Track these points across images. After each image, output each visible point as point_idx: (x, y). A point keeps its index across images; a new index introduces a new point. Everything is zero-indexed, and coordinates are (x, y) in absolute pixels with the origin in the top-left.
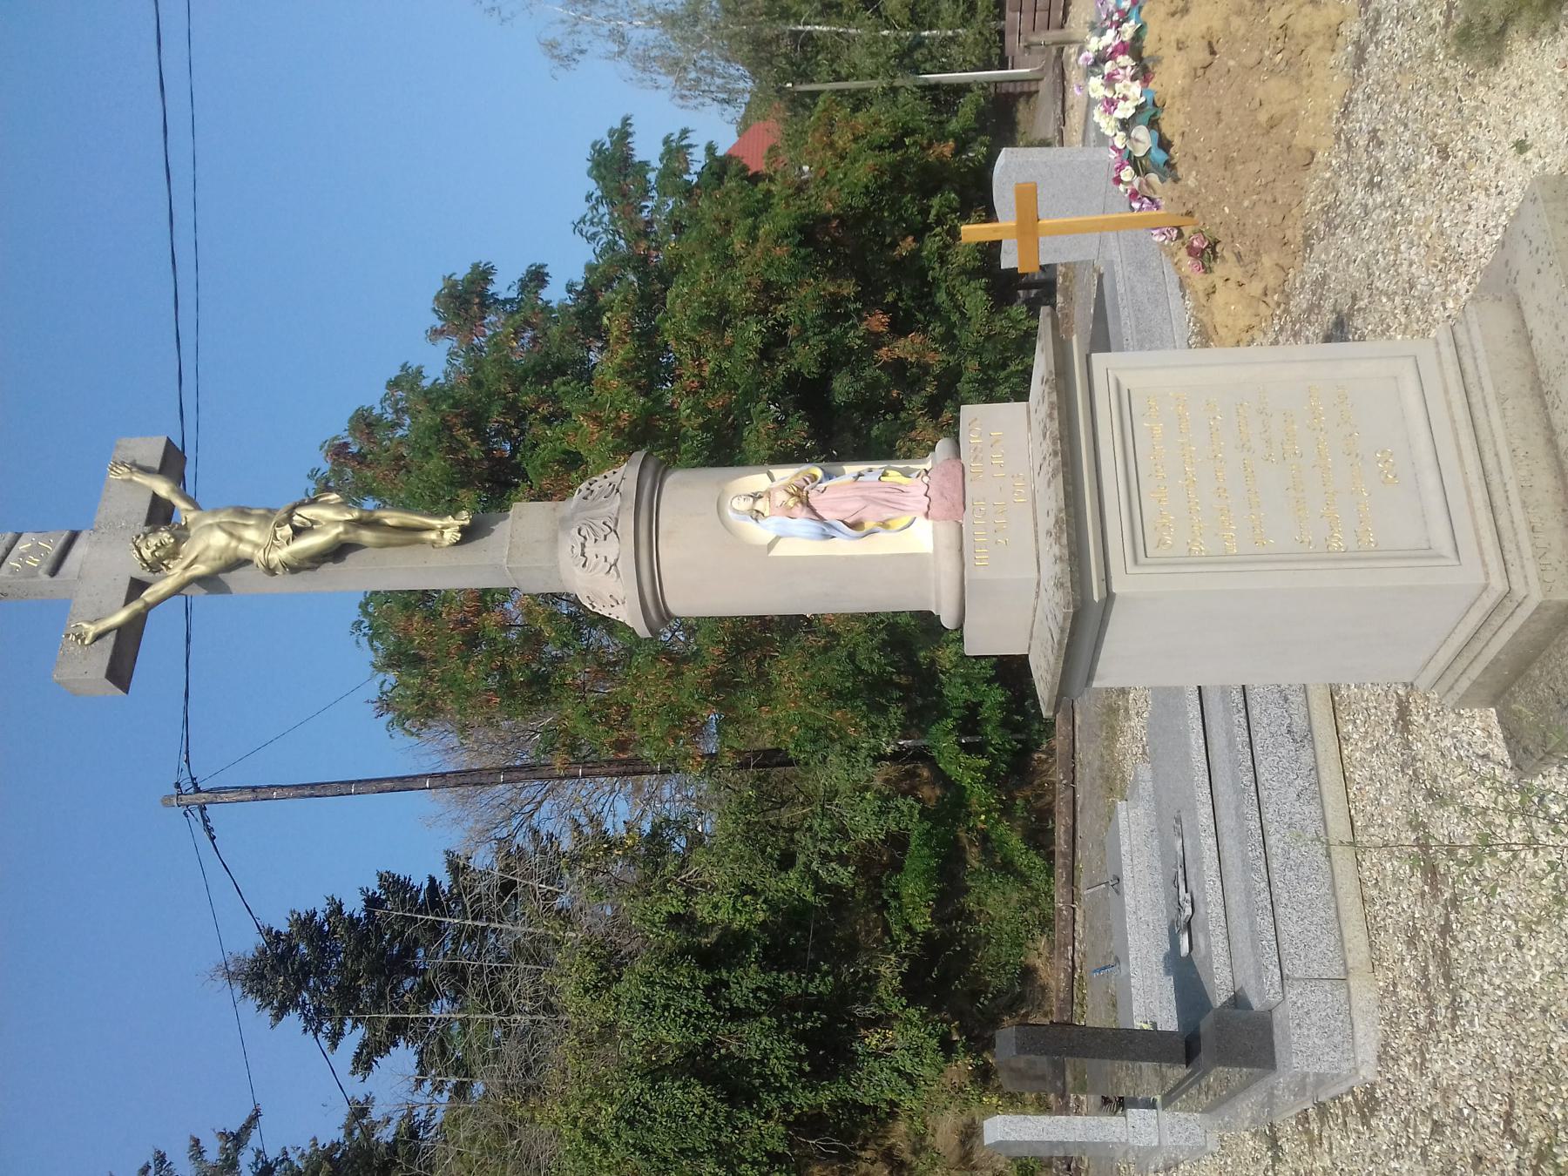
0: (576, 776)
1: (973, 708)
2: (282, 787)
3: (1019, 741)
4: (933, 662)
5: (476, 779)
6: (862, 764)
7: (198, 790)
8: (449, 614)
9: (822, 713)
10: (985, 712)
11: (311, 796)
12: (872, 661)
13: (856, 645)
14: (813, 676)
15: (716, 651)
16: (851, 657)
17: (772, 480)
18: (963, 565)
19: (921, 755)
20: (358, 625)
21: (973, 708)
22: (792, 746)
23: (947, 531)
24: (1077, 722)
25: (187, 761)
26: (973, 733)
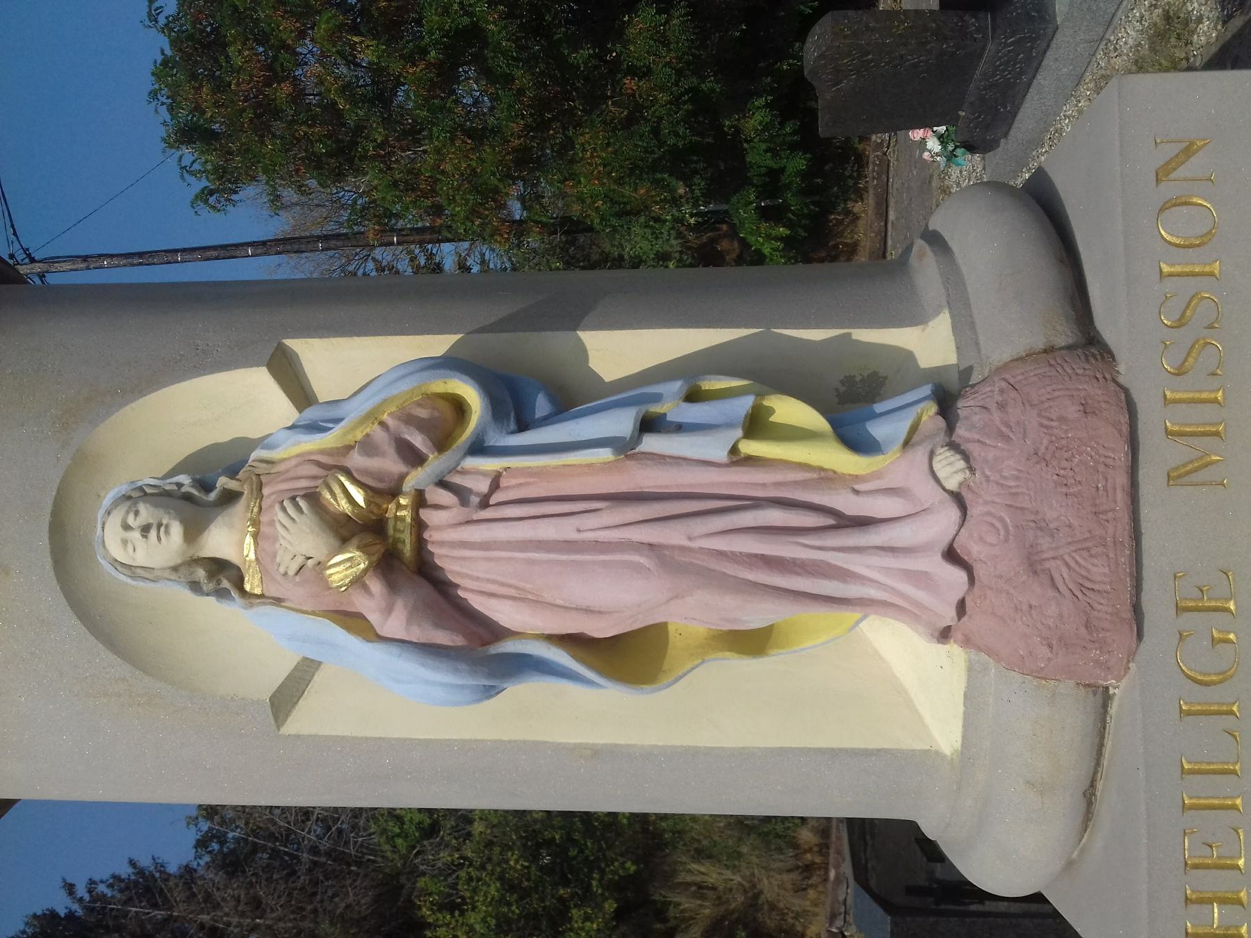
0: (392, 244)
1: (774, 174)
2: (112, 256)
3: (813, 203)
4: (738, 131)
5: (296, 247)
6: (665, 236)
7: (33, 260)
8: (238, 84)
9: (627, 191)
10: (785, 179)
11: (140, 264)
12: (677, 134)
13: (660, 119)
14: (615, 152)
15: (516, 127)
16: (656, 132)
17: (300, 393)
18: (1098, 763)
19: (722, 217)
20: (154, 94)
21: (774, 174)
22: (598, 221)
23: (1072, 716)
24: (892, 216)
25: (15, 234)
26: (772, 196)
